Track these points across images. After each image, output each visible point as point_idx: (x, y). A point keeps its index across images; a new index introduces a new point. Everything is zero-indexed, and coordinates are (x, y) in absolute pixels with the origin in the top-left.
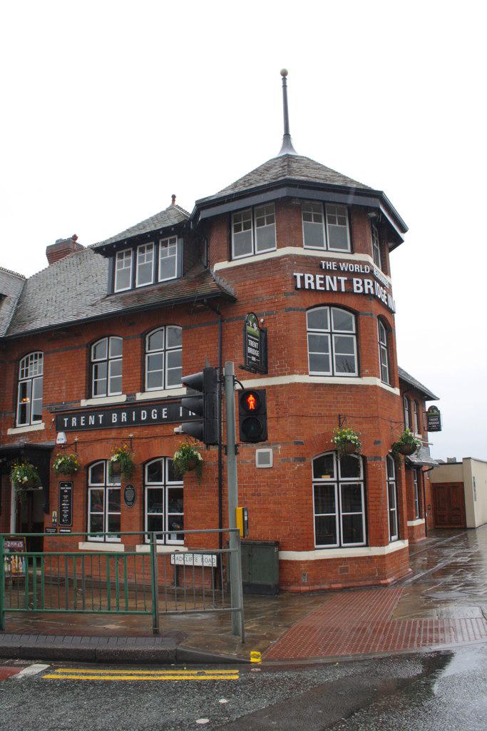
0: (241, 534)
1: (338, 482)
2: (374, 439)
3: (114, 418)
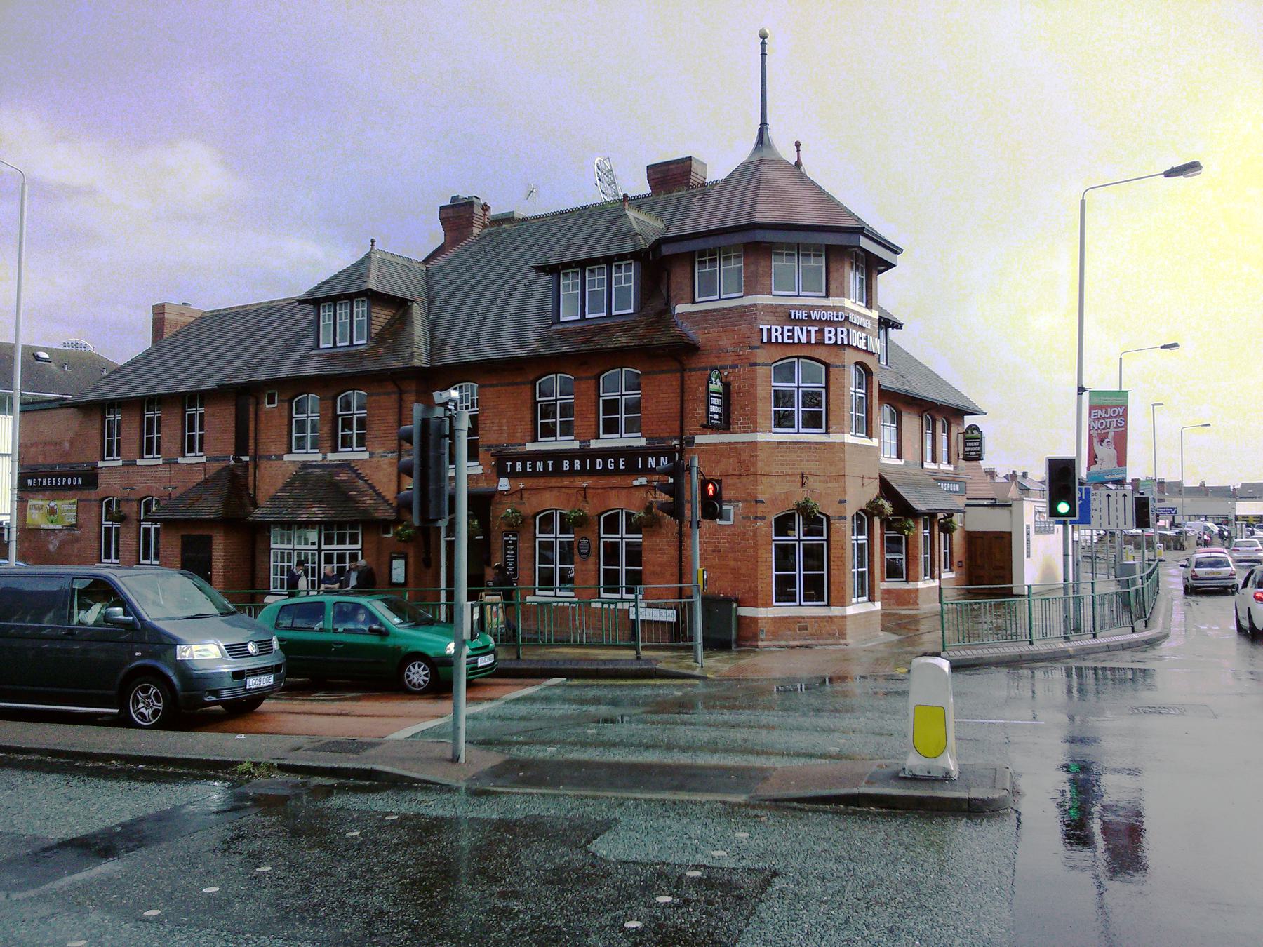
0: (702, 588)
1: (799, 540)
2: (839, 498)
3: (566, 465)
